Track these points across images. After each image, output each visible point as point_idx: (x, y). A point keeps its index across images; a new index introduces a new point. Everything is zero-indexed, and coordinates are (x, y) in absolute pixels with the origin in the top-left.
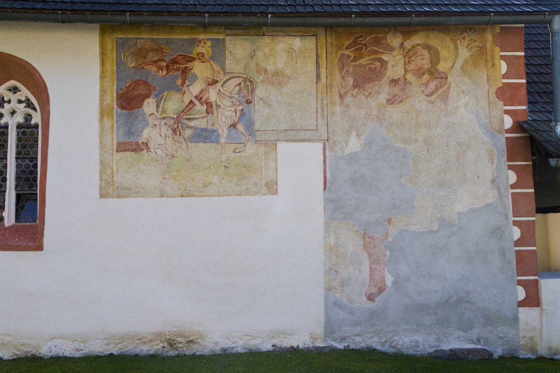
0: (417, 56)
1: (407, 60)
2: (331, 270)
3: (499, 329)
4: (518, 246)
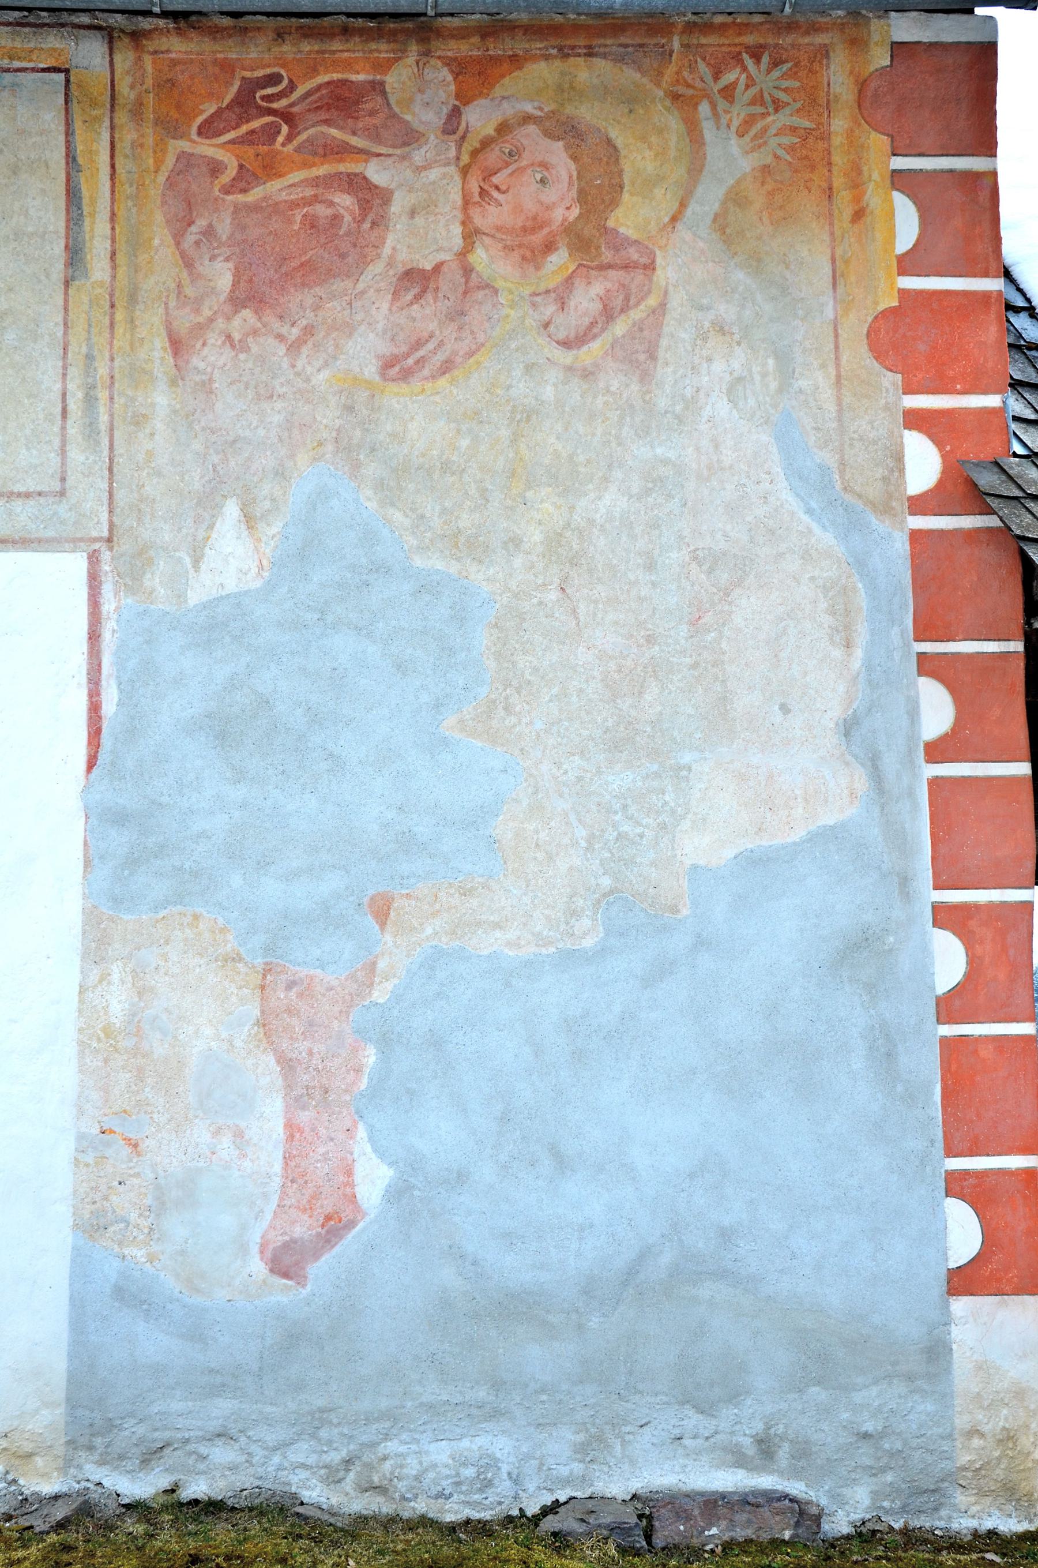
0: (521, 170)
1: (474, 186)
2: (109, 1140)
3: (858, 1397)
4: (951, 1020)
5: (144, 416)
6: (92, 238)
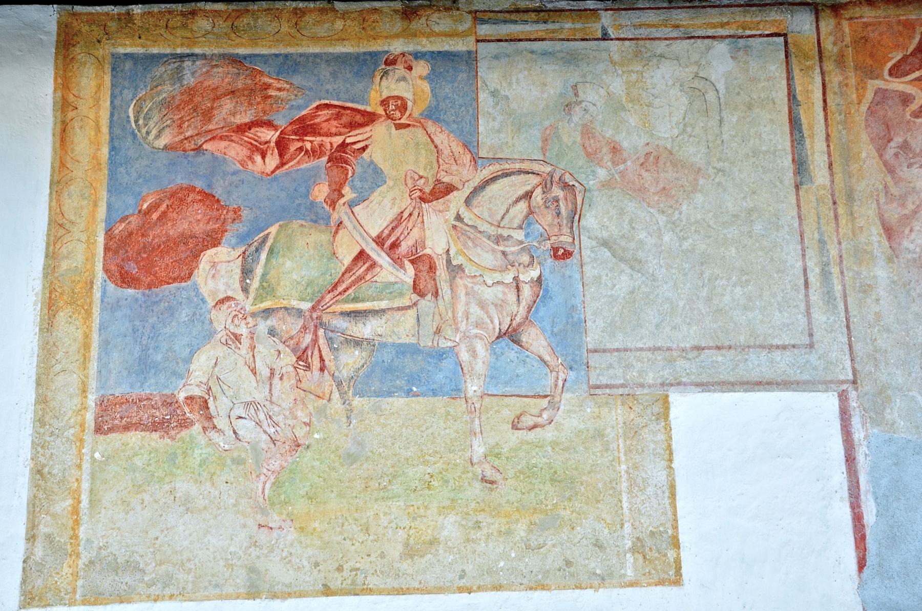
5: (869, 286)
6: (813, 154)
